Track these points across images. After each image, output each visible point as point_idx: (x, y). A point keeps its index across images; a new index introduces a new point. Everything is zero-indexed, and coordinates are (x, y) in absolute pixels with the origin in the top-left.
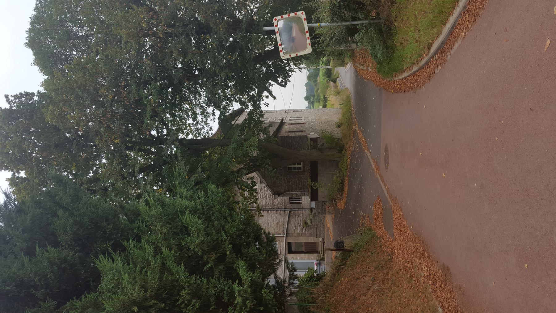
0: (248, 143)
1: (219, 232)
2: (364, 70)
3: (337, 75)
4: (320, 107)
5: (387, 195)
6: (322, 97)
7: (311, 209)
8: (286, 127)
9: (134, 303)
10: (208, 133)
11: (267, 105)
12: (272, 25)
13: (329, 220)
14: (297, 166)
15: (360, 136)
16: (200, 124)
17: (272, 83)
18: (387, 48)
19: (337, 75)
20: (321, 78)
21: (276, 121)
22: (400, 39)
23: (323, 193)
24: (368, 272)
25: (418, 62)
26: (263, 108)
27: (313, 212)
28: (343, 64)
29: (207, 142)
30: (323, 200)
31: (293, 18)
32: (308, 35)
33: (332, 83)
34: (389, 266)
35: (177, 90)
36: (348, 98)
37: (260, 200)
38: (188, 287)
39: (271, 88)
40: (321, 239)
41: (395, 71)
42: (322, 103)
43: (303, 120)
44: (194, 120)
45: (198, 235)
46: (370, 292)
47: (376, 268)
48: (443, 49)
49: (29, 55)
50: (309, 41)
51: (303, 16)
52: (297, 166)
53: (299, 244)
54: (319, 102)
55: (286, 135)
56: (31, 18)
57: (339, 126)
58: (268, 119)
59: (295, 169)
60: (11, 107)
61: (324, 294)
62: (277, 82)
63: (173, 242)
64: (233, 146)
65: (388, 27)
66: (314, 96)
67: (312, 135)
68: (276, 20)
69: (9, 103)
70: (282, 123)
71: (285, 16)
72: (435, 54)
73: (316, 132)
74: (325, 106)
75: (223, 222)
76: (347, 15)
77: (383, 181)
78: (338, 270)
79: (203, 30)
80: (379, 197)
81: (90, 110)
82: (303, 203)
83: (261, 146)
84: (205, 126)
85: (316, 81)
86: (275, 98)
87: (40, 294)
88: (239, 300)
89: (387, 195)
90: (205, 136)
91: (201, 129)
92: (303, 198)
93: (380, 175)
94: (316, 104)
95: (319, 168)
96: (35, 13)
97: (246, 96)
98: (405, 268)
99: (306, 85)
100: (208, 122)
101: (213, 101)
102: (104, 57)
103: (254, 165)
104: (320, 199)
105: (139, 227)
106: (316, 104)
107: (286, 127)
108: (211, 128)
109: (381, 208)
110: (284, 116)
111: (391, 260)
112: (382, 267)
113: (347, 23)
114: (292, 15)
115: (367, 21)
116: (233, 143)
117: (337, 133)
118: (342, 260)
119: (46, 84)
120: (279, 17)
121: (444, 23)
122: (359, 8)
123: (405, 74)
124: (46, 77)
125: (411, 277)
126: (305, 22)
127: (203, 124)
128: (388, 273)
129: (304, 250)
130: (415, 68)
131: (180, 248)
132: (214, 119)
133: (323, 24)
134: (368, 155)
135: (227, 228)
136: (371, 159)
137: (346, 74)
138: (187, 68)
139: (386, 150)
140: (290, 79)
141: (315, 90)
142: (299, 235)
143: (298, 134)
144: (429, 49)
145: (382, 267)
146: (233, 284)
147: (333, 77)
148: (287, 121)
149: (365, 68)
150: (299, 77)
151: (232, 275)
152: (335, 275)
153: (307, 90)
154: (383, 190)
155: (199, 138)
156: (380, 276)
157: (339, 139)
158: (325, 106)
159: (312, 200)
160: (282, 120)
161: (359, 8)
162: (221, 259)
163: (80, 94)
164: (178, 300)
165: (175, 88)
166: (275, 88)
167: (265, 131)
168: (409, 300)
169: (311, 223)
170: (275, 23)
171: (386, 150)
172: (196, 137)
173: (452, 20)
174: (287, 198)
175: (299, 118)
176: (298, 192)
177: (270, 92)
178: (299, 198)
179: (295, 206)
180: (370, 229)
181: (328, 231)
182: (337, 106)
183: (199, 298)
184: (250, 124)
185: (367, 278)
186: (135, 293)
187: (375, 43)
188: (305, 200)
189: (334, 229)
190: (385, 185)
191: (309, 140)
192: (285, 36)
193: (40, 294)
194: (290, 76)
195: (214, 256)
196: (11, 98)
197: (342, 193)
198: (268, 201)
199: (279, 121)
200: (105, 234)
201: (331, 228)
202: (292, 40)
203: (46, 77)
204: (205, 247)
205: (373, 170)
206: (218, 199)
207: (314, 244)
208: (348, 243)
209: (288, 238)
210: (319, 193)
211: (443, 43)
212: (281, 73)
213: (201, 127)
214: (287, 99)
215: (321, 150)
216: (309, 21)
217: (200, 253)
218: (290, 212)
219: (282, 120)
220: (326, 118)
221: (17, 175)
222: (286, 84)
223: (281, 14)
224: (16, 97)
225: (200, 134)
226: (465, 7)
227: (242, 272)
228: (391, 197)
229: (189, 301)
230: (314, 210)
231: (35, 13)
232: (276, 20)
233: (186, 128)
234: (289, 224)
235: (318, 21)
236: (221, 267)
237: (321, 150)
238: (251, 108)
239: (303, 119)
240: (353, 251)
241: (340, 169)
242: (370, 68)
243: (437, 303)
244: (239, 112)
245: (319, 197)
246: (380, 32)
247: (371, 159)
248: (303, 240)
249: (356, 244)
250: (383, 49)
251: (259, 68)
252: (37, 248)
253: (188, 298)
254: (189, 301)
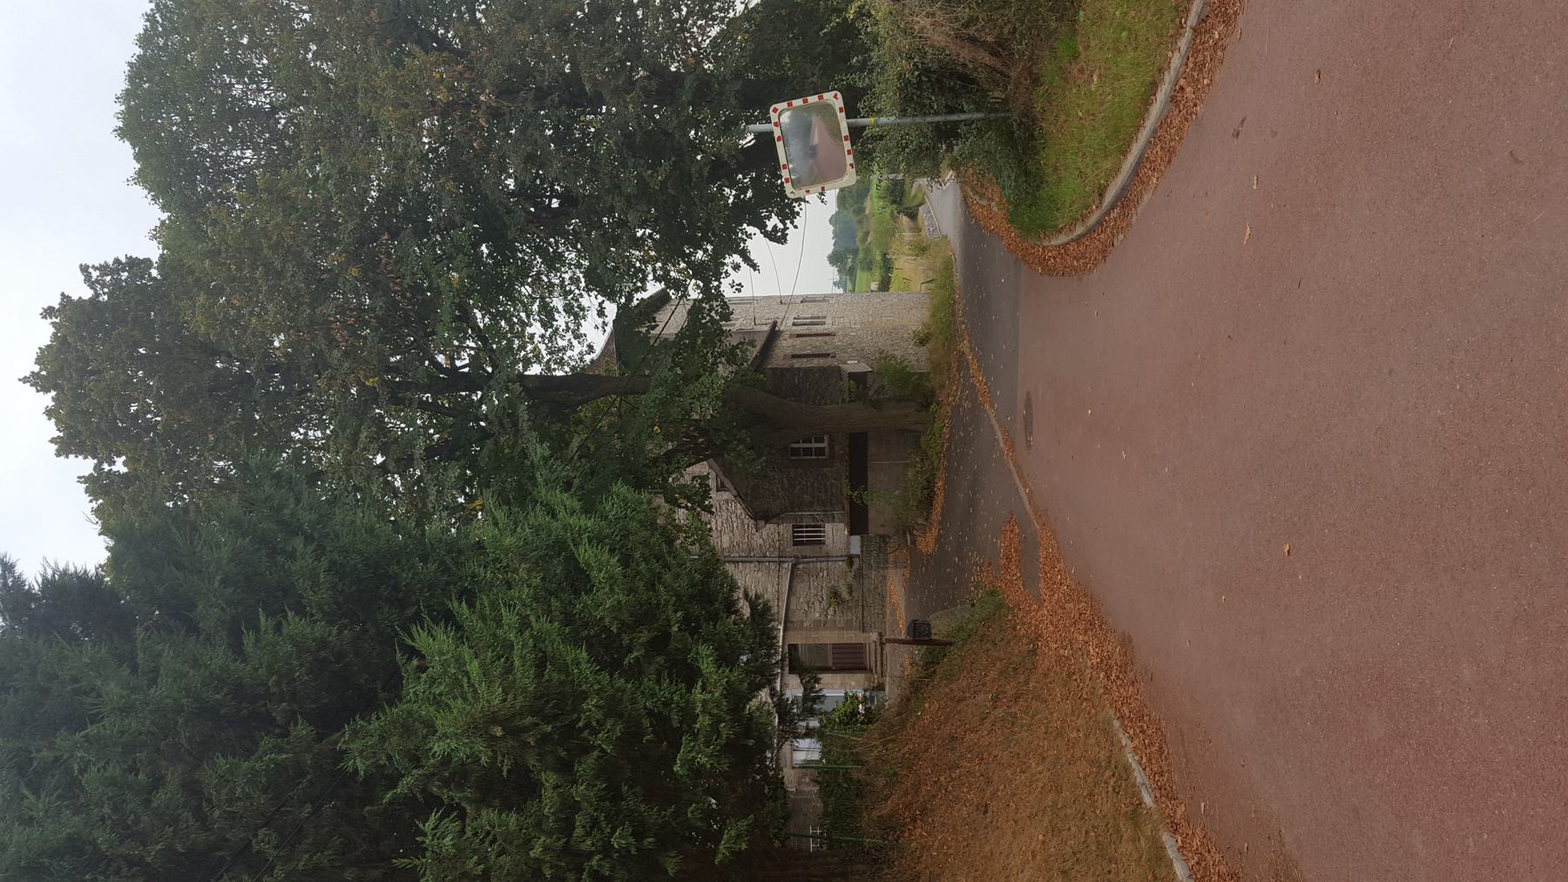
1: (651, 587)
4: (874, 286)
6: (879, 258)
7: (850, 559)
8: (784, 344)
9: (493, 719)
10: (581, 360)
12: (768, 121)
13: (896, 586)
14: (814, 445)
15: (974, 366)
16: (562, 337)
17: (751, 229)
18: (1027, 173)
20: (874, 204)
21: (758, 328)
23: (880, 513)
25: (1084, 218)
26: (728, 292)
27: (856, 566)
28: (934, 174)
29: (583, 382)
31: (814, 105)
32: (847, 145)
34: (1029, 666)
35: (504, 248)
36: (948, 265)
38: (598, 692)
40: (874, 636)
41: (1044, 227)
42: (877, 273)
43: (828, 326)
45: (611, 590)
46: (987, 725)
47: (1001, 673)
48: (1125, 200)
49: (125, 158)
50: (850, 159)
51: (838, 103)
52: (814, 445)
53: (819, 648)
54: (870, 269)
55: (786, 364)
56: (130, 64)
57: (922, 342)
58: (740, 321)
59: (808, 451)
60: (97, 295)
63: (555, 603)
66: (855, 252)
67: (853, 365)
68: (775, 110)
69: (92, 285)
70: (774, 334)
71: (798, 102)
72: (1112, 207)
73: (863, 357)
74: (885, 285)
75: (656, 566)
76: (937, 102)
77: (1021, 477)
78: (916, 689)
79: (576, 96)
81: (475, 328)
84: (575, 342)
85: (860, 211)
86: (754, 266)
87: (279, 710)
88: (703, 721)
90: (573, 368)
91: (564, 349)
92: (828, 527)
93: (1015, 462)
94: (861, 275)
95: (872, 450)
96: (139, 51)
97: (683, 265)
98: (1059, 659)
101: (600, 282)
104: (874, 529)
105: (474, 576)
106: (861, 275)
107: (784, 344)
108: (590, 347)
109: (1016, 540)
111: (1034, 652)
113: (938, 118)
114: (813, 99)
115: (980, 115)
116: (656, 387)
117: (917, 358)
118: (927, 665)
119: (164, 233)
120: (784, 105)
121: (1125, 153)
122: (963, 87)
123: (1062, 239)
124: (165, 216)
125: (1069, 675)
126: (842, 116)
127: (569, 335)
128: (1027, 682)
130: (1080, 230)
131: (568, 619)
132: (605, 324)
133: (883, 120)
135: (667, 577)
136: (996, 427)
137: (942, 202)
141: (860, 235)
142: (818, 625)
143: (816, 362)
144: (1101, 195)
146: (689, 691)
148: (786, 326)
149: (984, 202)
150: (817, 217)
151: (690, 675)
153: (836, 235)
155: (559, 373)
156: (1010, 689)
157: (921, 375)
158: (885, 285)
159: (852, 533)
160: (775, 324)
161: (963, 87)
162: (659, 643)
163: (277, 264)
164: (579, 719)
165: (501, 243)
166: (757, 243)
167: (731, 356)
169: (850, 593)
170: (774, 117)
173: (1136, 149)
174: (786, 529)
175: (817, 320)
177: (744, 254)
179: (807, 550)
180: (992, 593)
182: (918, 286)
183: (620, 716)
184: (694, 337)
185: (980, 697)
186: (492, 697)
187: (1001, 162)
188: (836, 534)
190: (1025, 486)
191: (846, 379)
192: (796, 147)
195: (645, 636)
196: (95, 274)
197: (929, 514)
198: (737, 538)
199: (766, 328)
200: (389, 598)
201: (902, 604)
202: (812, 152)
203: (165, 216)
204: (625, 616)
205: (1002, 453)
206: (641, 516)
207: (858, 649)
208: (940, 626)
209: (790, 633)
210: (872, 514)
212: (772, 204)
213: (565, 343)
214: (787, 272)
215: (877, 405)
216: (851, 111)
218: (794, 566)
219: (775, 324)
221: (106, 467)
223: (788, 98)
224: (104, 269)
225: (561, 363)
226: (1155, 131)
227: (707, 666)
229: (600, 723)
230: (856, 561)
231: (139, 51)
232: (775, 110)
233: (522, 347)
234: (793, 599)
235: (872, 111)
237: (877, 405)
238: (694, 294)
239: (829, 321)
240: (951, 644)
242: (994, 207)
243: (1112, 712)
245: (871, 525)
246: (1008, 138)
247: (996, 427)
248: (829, 637)
249: (960, 629)
250: (1018, 176)
251: (716, 199)
252: (262, 619)
254: (600, 723)
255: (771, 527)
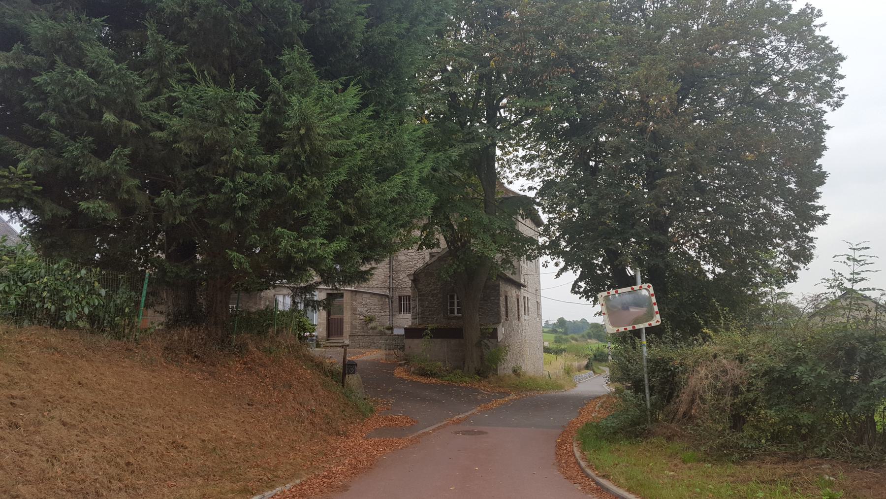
0: (488, 240)
1: (379, 215)
2: (594, 407)
3: (599, 371)
4: (546, 344)
5: (421, 432)
6: (563, 347)
7: (391, 328)
8: (514, 292)
9: (309, 129)
11: (545, 266)
13: (375, 355)
14: (456, 308)
15: (501, 401)
17: (579, 272)
18: (615, 433)
19: (599, 371)
20: (594, 345)
21: (522, 277)
22: (623, 448)
23: (417, 346)
24: (320, 405)
25: (590, 466)
26: (542, 259)
27: (387, 332)
28: (612, 379)
29: (492, 179)
30: (407, 347)
31: (652, 309)
32: (630, 328)
33: (585, 362)
35: (566, 135)
36: (560, 387)
37: (406, 251)
39: (570, 272)
40: (347, 342)
41: (584, 443)
42: (554, 346)
43: (524, 317)
44: (523, 157)
45: (378, 193)
46: (297, 406)
47: (326, 415)
50: (622, 329)
51: (654, 323)
52: (456, 308)
53: (341, 311)
55: (502, 292)
57: (515, 371)
58: (526, 266)
59: (452, 304)
61: (288, 347)
62: (581, 279)
64: (486, 220)
65: (641, 433)
66: (565, 333)
67: (501, 331)
68: (649, 287)
70: (519, 286)
71: (654, 299)
72: (597, 483)
73: (506, 336)
74: (547, 350)
76: (656, 380)
77: (438, 428)
78: (318, 365)
80: (417, 422)
82: (401, 316)
83: (483, 260)
84: (514, 174)
85: (590, 337)
86: (558, 275)
87: (316, 14)
89: (421, 432)
91: (510, 168)
92: (409, 316)
93: (447, 424)
94: (552, 337)
99: (584, 321)
100: (520, 178)
101: (548, 188)
102: (609, 43)
103: (458, 246)
104: (408, 342)
105: (387, 119)
106: (552, 337)
107: (514, 292)
108: (511, 183)
109: (402, 425)
110: (531, 288)
111: (338, 434)
112: (328, 423)
118: (331, 372)
120: (652, 290)
123: (578, 454)
125: (325, 455)
126: (646, 325)
127: (518, 171)
129: (332, 317)
130: (583, 464)
132: (524, 191)
133: (645, 349)
134: (473, 411)
137: (597, 384)
138: (598, 149)
139: (480, 433)
140: (583, 299)
141: (576, 336)
142: (354, 310)
144: (604, 476)
145: (328, 423)
147: (595, 364)
148: (523, 292)
149: (597, 409)
150: (586, 311)
151: (330, 237)
152: (312, 361)
153: (575, 322)
154: (426, 427)
155: (496, 165)
156: (317, 420)
157: (496, 370)
158: (547, 350)
159: (406, 329)
160: (525, 286)
162: (348, 220)
164: (307, 175)
165: (570, 134)
166: (571, 276)
167: (507, 261)
168: (299, 451)
169: (372, 328)
171: (480, 433)
172: (499, 159)
174: (408, 292)
176: (418, 310)
177: (564, 269)
178: (408, 310)
179: (396, 304)
180: (371, 411)
181: (360, 353)
182: (547, 370)
183: (308, 198)
185: (313, 402)
186: (321, 128)
188: (405, 320)
189: (367, 361)
190: (433, 430)
191: (494, 327)
192: (628, 298)
193: (316, 14)
194: (588, 298)
195: (352, 211)
197: (417, 374)
198: (403, 264)
199: (522, 282)
201: (365, 358)
202: (626, 307)
204: (363, 201)
205: (453, 417)
206: (418, 210)
207: (340, 333)
208: (353, 380)
210: (416, 341)
211: (608, 490)
212: (592, 285)
214: (554, 293)
215: (479, 344)
216: (649, 330)
217: (356, 195)
218: (387, 296)
219: (525, 286)
220: (528, 351)
222: (576, 293)
225: (502, 166)
227: (335, 246)
228: (419, 436)
230: (390, 332)
232: (649, 287)
233: (511, 145)
235: (649, 342)
236: (339, 220)
237: (479, 344)
239: (526, 317)
241: (452, 372)
242: (595, 415)
243: (304, 479)
244: (538, 222)
246: (635, 423)
248: (347, 316)
250: (613, 428)
253: (309, 186)
255: (410, 283)
